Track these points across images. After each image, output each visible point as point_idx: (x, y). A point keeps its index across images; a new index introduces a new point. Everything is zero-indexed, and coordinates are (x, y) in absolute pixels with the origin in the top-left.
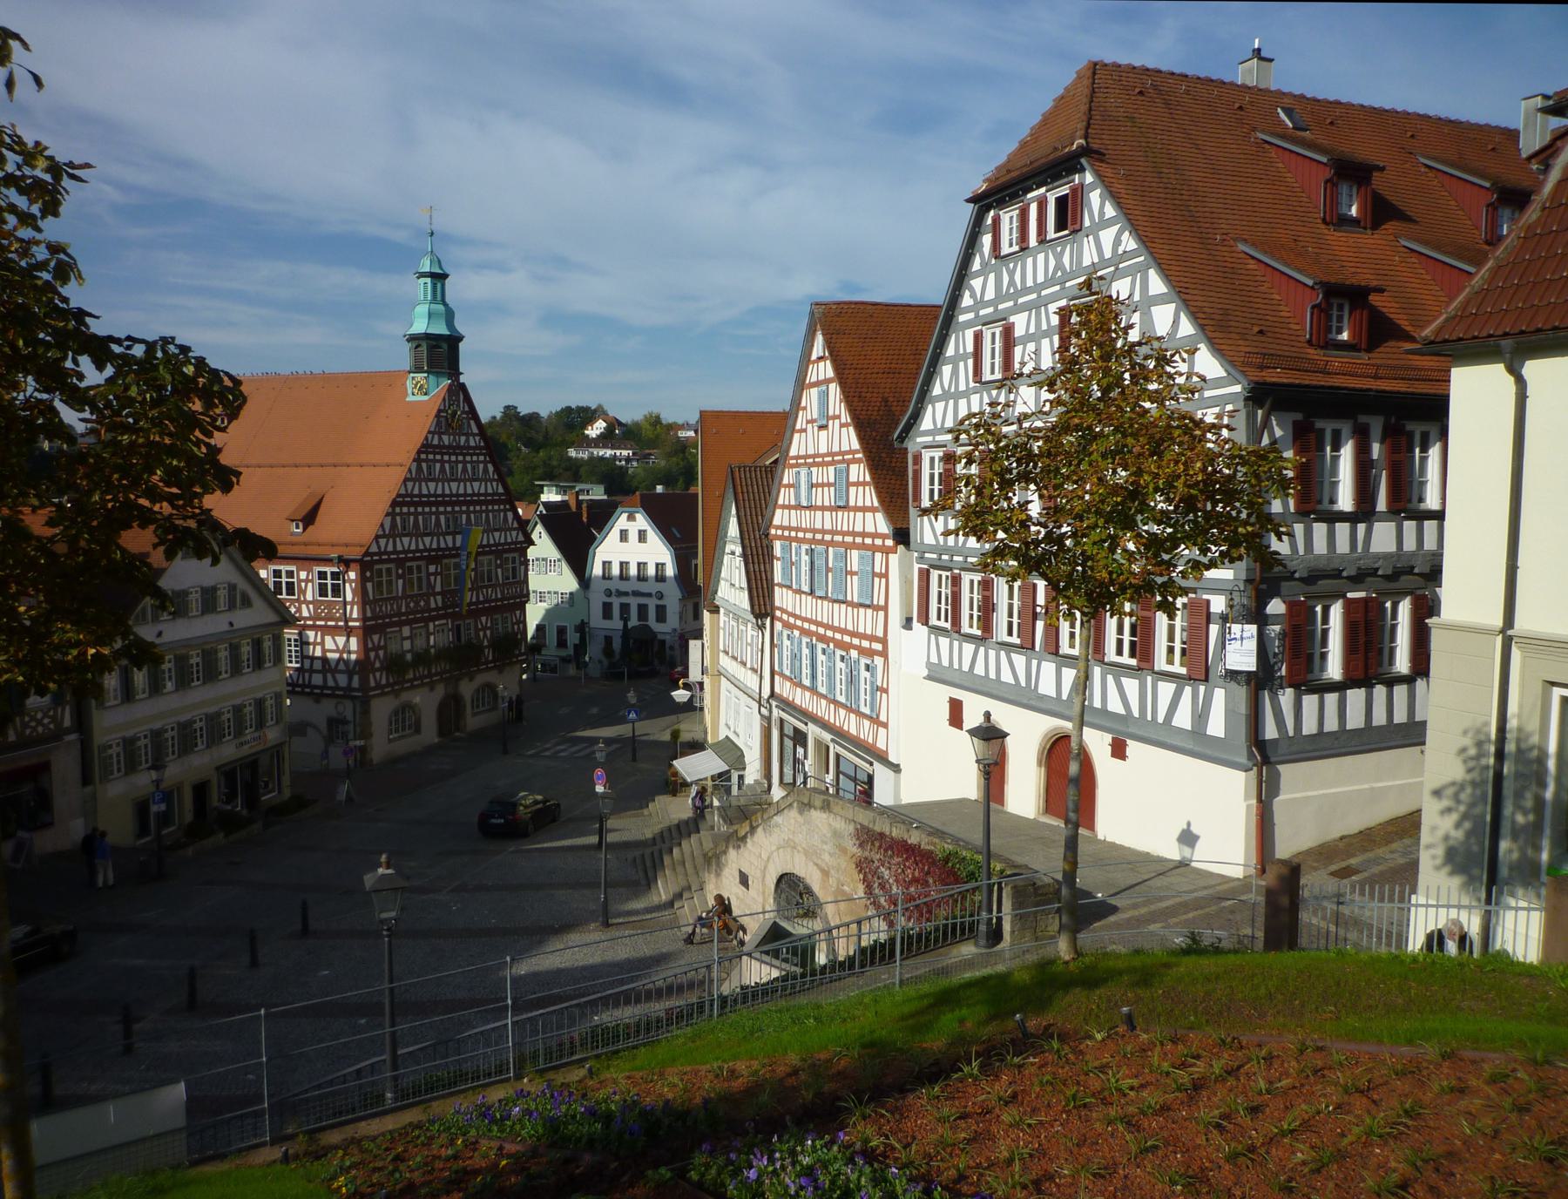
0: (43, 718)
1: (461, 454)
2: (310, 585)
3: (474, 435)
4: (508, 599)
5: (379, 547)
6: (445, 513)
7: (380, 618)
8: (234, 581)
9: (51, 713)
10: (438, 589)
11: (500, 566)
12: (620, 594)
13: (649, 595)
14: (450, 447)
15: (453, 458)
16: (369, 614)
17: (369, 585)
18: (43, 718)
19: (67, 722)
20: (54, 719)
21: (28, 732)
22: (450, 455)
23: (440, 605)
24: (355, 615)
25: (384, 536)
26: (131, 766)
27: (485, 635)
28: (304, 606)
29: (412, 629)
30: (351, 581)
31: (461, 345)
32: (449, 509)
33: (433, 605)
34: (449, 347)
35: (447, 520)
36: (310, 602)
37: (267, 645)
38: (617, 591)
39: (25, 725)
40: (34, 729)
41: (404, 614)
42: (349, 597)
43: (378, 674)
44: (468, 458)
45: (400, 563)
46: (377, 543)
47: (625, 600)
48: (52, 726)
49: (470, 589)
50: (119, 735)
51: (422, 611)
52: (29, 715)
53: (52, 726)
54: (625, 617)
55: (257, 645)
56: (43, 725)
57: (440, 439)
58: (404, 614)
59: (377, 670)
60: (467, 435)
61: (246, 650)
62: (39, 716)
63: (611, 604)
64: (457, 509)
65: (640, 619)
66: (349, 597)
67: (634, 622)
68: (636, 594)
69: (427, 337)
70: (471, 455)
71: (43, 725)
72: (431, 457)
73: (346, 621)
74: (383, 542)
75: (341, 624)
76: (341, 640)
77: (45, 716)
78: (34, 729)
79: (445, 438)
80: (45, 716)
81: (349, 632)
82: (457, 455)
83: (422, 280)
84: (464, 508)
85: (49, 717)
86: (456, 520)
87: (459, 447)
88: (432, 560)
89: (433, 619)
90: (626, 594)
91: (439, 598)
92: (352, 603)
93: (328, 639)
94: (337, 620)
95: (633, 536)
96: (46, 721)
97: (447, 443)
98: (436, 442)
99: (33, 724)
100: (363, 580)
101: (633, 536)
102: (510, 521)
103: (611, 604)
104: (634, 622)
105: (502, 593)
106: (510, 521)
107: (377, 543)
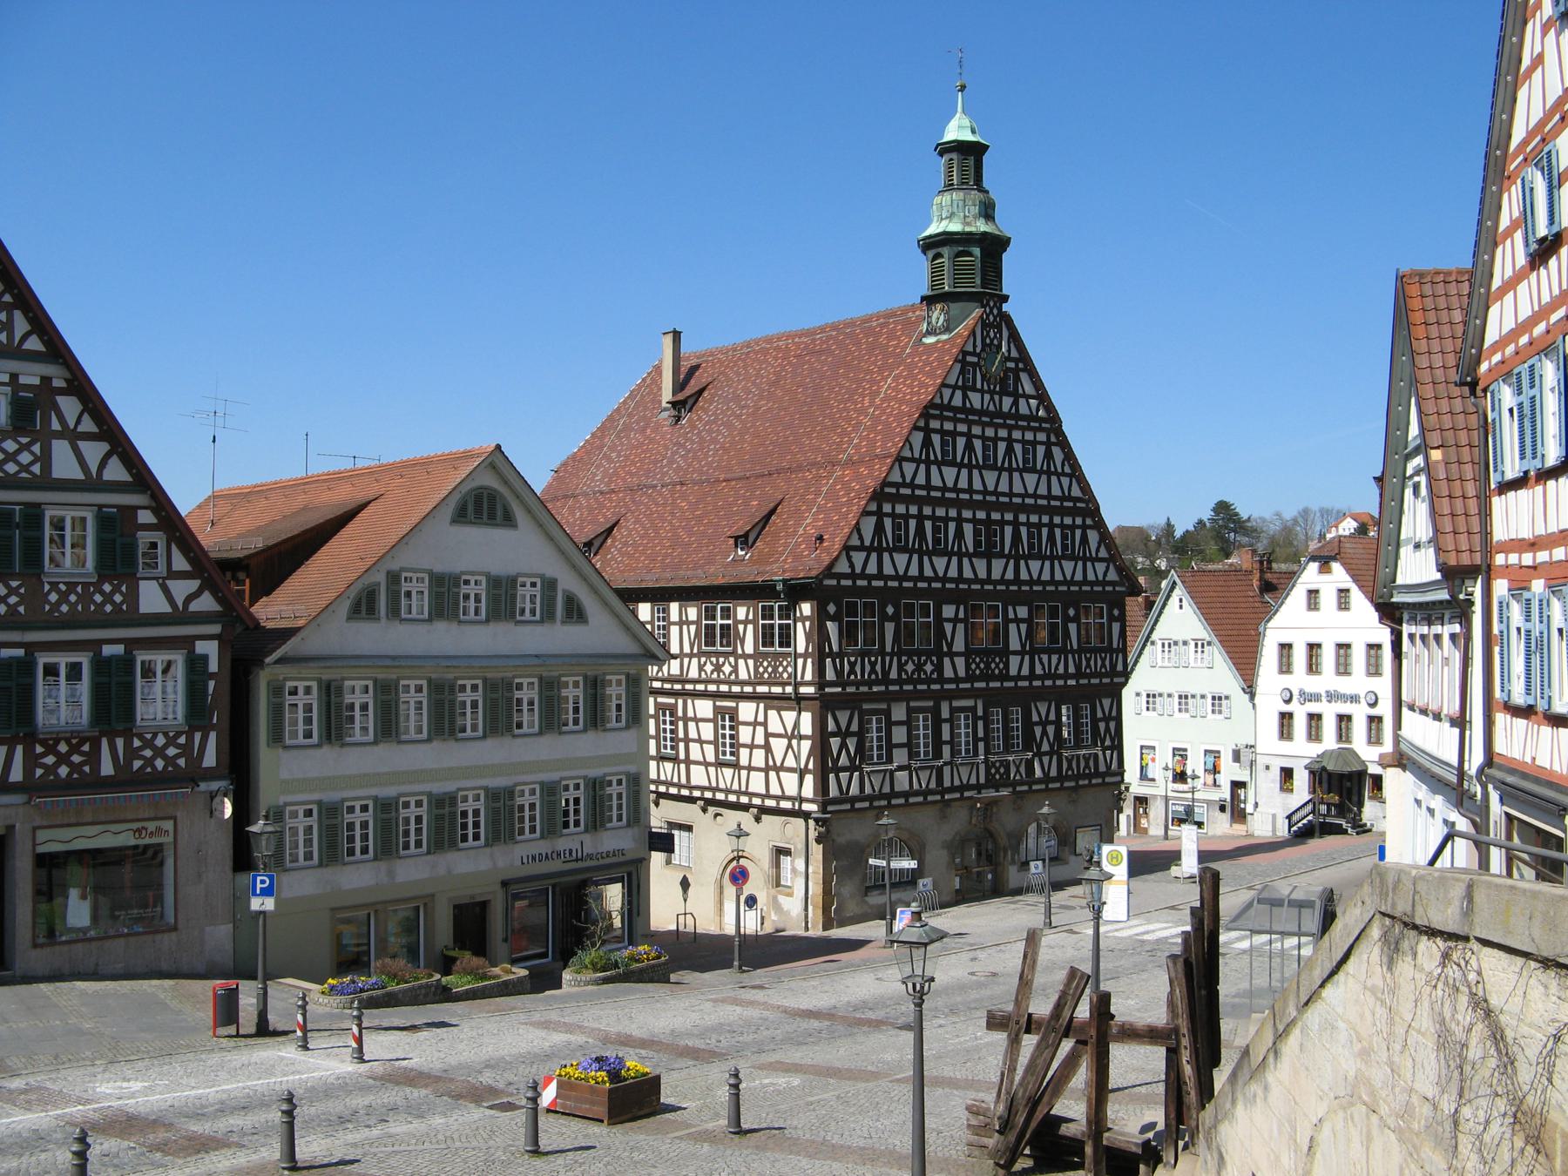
0: (166, 746)
1: (1004, 426)
2: (750, 627)
3: (1028, 397)
4: (1089, 676)
5: (852, 566)
6: (974, 521)
7: (1085, 676)
8: (550, 572)
9: (182, 740)
10: (959, 645)
11: (1076, 619)
12: (1308, 697)
13: (1354, 699)
14: (982, 413)
15: (990, 432)
16: (830, 675)
17: (831, 627)
18: (166, 746)
19: (210, 760)
20: (186, 750)
21: (137, 764)
22: (984, 425)
23: (962, 673)
24: (808, 676)
25: (861, 548)
26: (333, 849)
27: (1045, 733)
28: (741, 662)
29: (910, 711)
30: (803, 619)
31: (1007, 258)
32: (981, 515)
33: (948, 672)
34: (985, 254)
35: (977, 533)
36: (750, 656)
37: (616, 692)
38: (1302, 693)
39: (132, 753)
40: (150, 762)
41: (893, 682)
42: (801, 648)
43: (844, 776)
44: (1017, 435)
45: (886, 595)
46: (849, 558)
47: (1313, 707)
48: (182, 762)
49: (1022, 653)
50: (316, 796)
51: (929, 681)
52: (141, 737)
53: (182, 762)
54: (1314, 733)
55: (595, 687)
56: (165, 757)
57: (965, 397)
58: (893, 682)
59: (844, 769)
60: (1016, 396)
61: (573, 693)
62: (160, 741)
63: (1290, 715)
64: (996, 516)
65: (1340, 738)
66: (801, 645)
67: (1329, 741)
68: (1332, 697)
69: (946, 239)
70: (1023, 429)
71: (165, 757)
72: (948, 426)
73: (797, 685)
74: (859, 558)
75: (789, 689)
76: (790, 716)
77: (171, 742)
78: (150, 762)
79: (975, 399)
80: (171, 742)
81: (798, 702)
82: (997, 426)
83: (946, 157)
84: (1009, 517)
85: (178, 746)
86: (990, 534)
87: (999, 413)
88: (957, 598)
89: (951, 696)
90: (1315, 698)
91: (960, 662)
92: (805, 656)
93: (772, 714)
94: (784, 684)
95: (1328, 599)
96: (172, 751)
97: (977, 405)
98: (957, 401)
99: (148, 753)
100: (821, 616)
101: (1328, 599)
102: (1093, 546)
103: (1290, 715)
104: (1329, 741)
105: (1078, 666)
106: (1093, 546)
107: (849, 558)
